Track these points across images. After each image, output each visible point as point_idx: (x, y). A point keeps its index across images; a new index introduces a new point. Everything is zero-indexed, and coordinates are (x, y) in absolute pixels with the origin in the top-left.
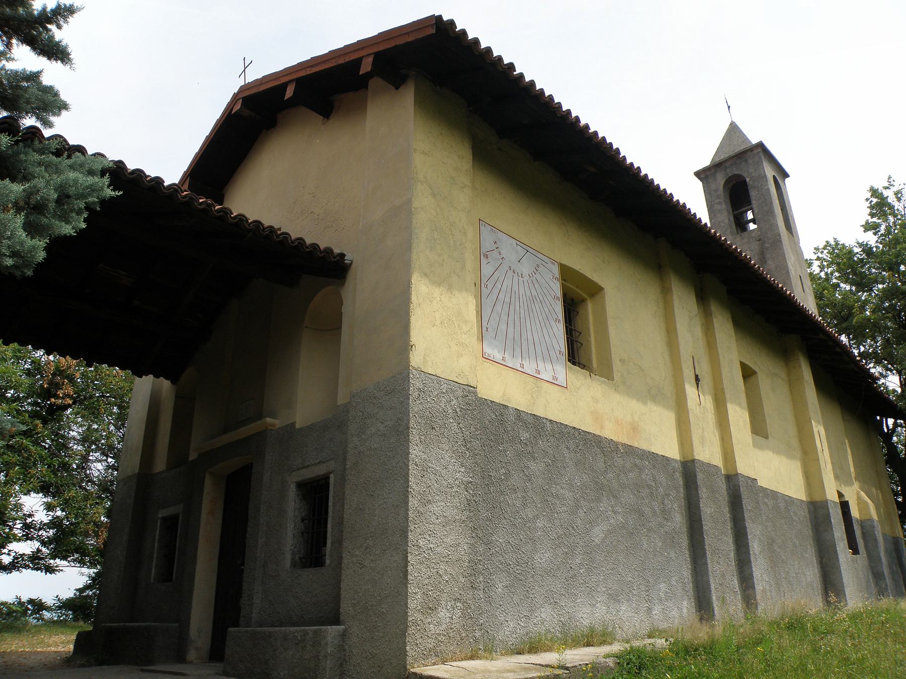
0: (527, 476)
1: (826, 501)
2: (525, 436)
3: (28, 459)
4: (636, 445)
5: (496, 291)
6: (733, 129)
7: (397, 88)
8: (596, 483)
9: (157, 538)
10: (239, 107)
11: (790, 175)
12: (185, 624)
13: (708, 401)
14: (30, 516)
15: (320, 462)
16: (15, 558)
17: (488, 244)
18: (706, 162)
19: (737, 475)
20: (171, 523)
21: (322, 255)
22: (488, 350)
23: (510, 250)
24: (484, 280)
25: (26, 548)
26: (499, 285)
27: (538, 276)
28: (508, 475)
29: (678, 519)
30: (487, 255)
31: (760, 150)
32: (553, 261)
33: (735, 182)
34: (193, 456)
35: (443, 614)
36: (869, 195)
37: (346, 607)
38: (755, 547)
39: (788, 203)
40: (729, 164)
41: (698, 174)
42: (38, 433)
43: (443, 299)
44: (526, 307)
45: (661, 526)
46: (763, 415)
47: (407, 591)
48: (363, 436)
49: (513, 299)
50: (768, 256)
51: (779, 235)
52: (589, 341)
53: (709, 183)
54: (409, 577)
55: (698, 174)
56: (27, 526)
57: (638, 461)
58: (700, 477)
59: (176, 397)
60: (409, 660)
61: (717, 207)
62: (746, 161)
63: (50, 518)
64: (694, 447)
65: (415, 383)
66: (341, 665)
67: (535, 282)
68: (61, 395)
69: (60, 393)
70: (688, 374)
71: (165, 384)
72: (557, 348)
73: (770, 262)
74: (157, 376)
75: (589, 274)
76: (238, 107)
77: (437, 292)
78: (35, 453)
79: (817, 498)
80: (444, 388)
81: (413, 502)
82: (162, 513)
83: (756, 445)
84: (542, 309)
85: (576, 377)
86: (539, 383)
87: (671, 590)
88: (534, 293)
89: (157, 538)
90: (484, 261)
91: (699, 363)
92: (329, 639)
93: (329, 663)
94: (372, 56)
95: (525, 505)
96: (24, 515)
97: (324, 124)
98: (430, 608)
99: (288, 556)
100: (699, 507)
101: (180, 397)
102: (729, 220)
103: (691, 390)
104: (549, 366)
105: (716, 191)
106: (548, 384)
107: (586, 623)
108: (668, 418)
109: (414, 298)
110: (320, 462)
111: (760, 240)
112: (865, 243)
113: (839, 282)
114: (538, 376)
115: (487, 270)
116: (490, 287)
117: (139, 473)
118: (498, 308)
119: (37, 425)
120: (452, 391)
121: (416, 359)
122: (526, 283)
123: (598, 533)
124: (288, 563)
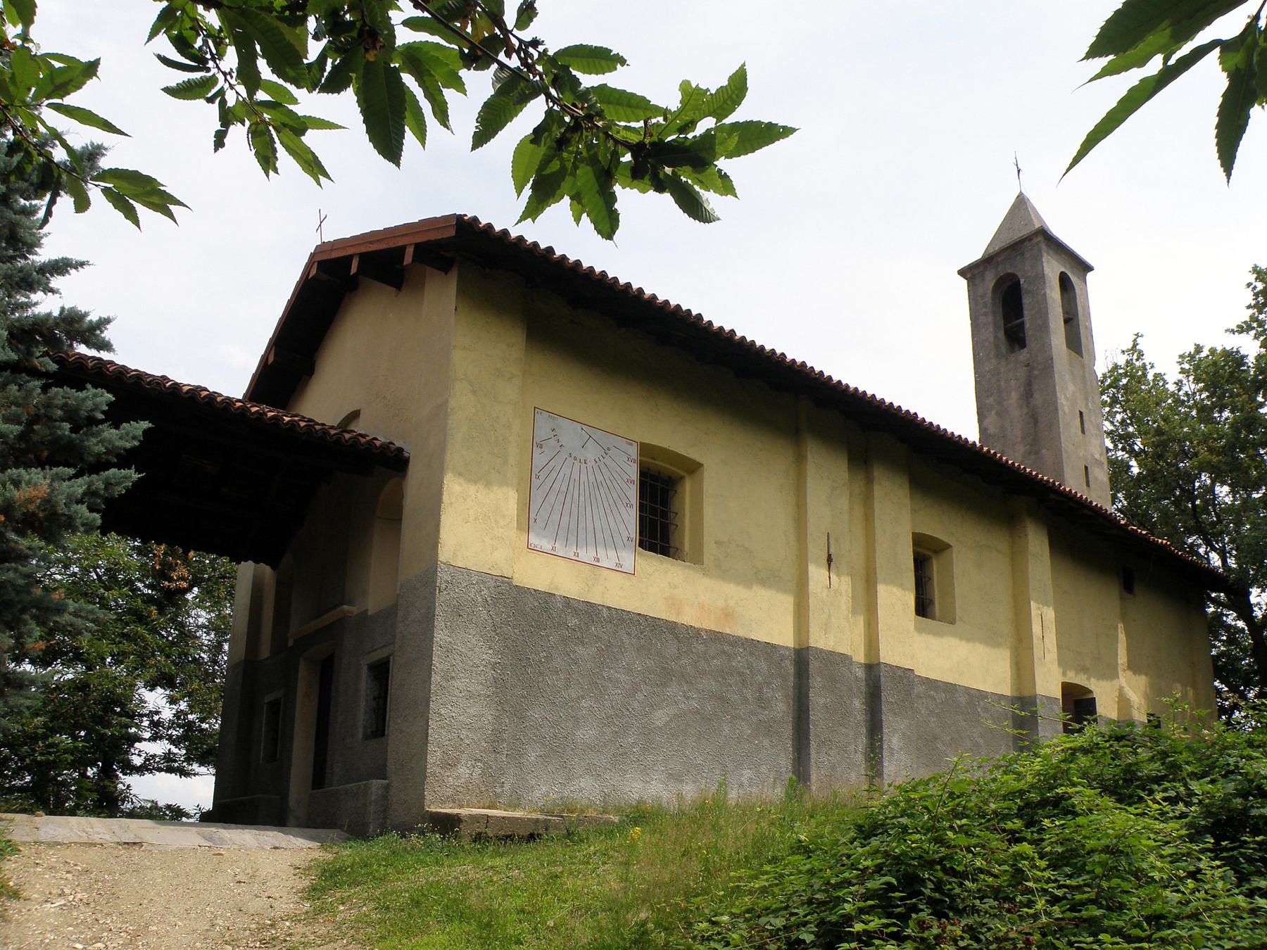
0: (573, 659)
1: (1035, 696)
2: (573, 622)
3: (145, 648)
4: (728, 631)
5: (549, 482)
6: (1021, 205)
7: (446, 274)
8: (664, 668)
9: (264, 722)
10: (315, 272)
11: (1095, 268)
12: (284, 796)
13: (843, 584)
14: (157, 713)
15: (385, 646)
16: (147, 760)
17: (543, 431)
18: (976, 254)
19: (879, 664)
20: (275, 706)
21: (379, 451)
22: (534, 540)
23: (570, 435)
24: (535, 471)
25: (159, 748)
26: (554, 475)
27: (608, 461)
28: (549, 658)
29: (781, 707)
30: (541, 445)
31: (1040, 238)
32: (630, 441)
33: (1010, 283)
34: (290, 644)
35: (462, 770)
36: (1252, 278)
37: (391, 767)
38: (894, 741)
41: (962, 273)
42: (153, 621)
43: (479, 495)
44: (587, 494)
45: (752, 713)
47: (427, 749)
48: (407, 623)
49: (571, 488)
50: (1035, 387)
51: (1052, 359)
52: (683, 523)
53: (976, 285)
54: (429, 738)
55: (962, 273)
56: (155, 724)
57: (727, 648)
58: (814, 665)
59: (277, 583)
60: (427, 802)
61: (982, 319)
62: (1022, 254)
63: (174, 712)
64: (811, 634)
65: (443, 576)
66: (384, 811)
67: (603, 467)
68: (175, 578)
69: (174, 575)
70: (816, 550)
71: (267, 570)
72: (625, 534)
73: (1036, 395)
74: (256, 562)
75: (682, 451)
76: (313, 272)
77: (472, 489)
78: (151, 642)
79: (1026, 693)
80: (475, 579)
81: (436, 678)
82: (268, 698)
83: (919, 629)
84: (608, 494)
85: (653, 564)
86: (597, 570)
87: (758, 777)
88: (600, 478)
89: (264, 722)
90: (537, 451)
91: (837, 540)
92: (373, 789)
93: (372, 808)
94: (413, 246)
95: (567, 687)
96: (150, 711)
97: (396, 296)
98: (450, 764)
99: (361, 730)
100: (808, 697)
101: (280, 583)
102: (996, 337)
103: (817, 574)
104: (612, 553)
105: (983, 296)
107: (636, 796)
108: (785, 603)
109: (445, 498)
110: (385, 646)
111: (1028, 365)
112: (1235, 350)
114: (597, 564)
115: (540, 460)
116: (542, 477)
117: (245, 660)
118: (552, 498)
119: (151, 612)
120: (483, 582)
121: (444, 554)
122: (590, 470)
123: (660, 717)
124: (360, 736)
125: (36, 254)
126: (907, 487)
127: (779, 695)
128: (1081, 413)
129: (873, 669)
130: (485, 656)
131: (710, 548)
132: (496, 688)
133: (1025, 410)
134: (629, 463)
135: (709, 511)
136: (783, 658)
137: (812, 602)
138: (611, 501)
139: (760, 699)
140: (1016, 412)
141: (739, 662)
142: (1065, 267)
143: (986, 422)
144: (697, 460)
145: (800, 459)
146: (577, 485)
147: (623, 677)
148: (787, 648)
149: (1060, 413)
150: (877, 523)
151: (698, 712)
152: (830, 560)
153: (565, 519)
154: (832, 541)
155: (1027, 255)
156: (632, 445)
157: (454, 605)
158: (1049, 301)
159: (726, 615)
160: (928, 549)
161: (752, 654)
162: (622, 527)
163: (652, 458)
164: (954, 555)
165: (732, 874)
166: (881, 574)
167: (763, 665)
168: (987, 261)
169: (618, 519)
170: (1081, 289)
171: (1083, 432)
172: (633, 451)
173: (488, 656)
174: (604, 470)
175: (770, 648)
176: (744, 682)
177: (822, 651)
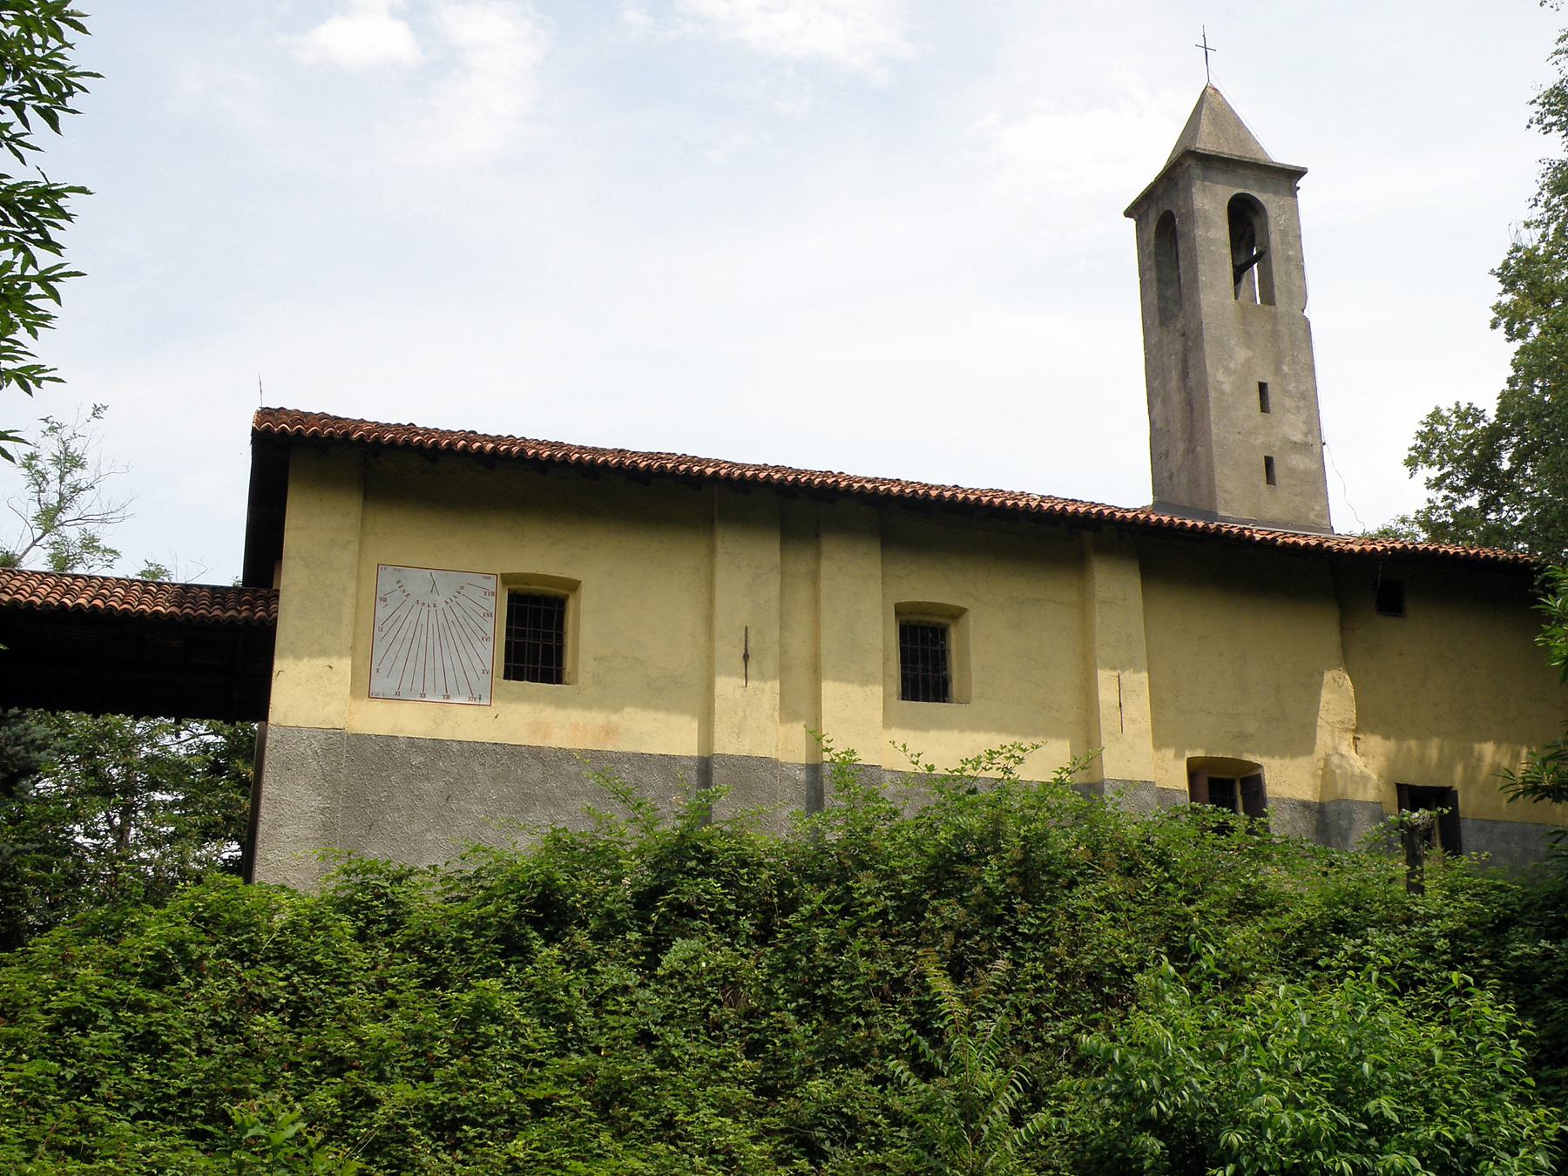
2: (417, 760)
6: (1209, 106)
31: (1190, 162)
32: (487, 576)
39: (1284, 233)
40: (1161, 191)
41: (1128, 214)
44: (436, 636)
46: (970, 670)
49: (418, 632)
50: (1190, 363)
55: (1128, 214)
58: (718, 773)
62: (1176, 184)
70: (728, 650)
72: (479, 668)
73: (1191, 375)
88: (451, 617)
95: (410, 822)
106: (467, 707)
111: (1183, 335)
113: (1529, 340)
115: (383, 613)
116: (385, 630)
118: (396, 646)
122: (440, 613)
125: (35, 334)
126: (876, 556)
128: (1263, 387)
130: (313, 803)
132: (325, 830)
133: (1183, 394)
134: (487, 597)
138: (464, 638)
140: (1177, 399)
143: (1155, 412)
144: (573, 577)
146: (424, 631)
147: (474, 808)
148: (691, 758)
149: (1212, 395)
152: (746, 657)
153: (411, 664)
156: (489, 578)
157: (284, 761)
158: (1201, 245)
159: (608, 732)
160: (940, 616)
162: (476, 661)
163: (526, 584)
164: (972, 622)
166: (826, 662)
167: (657, 779)
171: (1264, 407)
172: (491, 585)
173: (316, 802)
174: (457, 610)
175: (666, 763)
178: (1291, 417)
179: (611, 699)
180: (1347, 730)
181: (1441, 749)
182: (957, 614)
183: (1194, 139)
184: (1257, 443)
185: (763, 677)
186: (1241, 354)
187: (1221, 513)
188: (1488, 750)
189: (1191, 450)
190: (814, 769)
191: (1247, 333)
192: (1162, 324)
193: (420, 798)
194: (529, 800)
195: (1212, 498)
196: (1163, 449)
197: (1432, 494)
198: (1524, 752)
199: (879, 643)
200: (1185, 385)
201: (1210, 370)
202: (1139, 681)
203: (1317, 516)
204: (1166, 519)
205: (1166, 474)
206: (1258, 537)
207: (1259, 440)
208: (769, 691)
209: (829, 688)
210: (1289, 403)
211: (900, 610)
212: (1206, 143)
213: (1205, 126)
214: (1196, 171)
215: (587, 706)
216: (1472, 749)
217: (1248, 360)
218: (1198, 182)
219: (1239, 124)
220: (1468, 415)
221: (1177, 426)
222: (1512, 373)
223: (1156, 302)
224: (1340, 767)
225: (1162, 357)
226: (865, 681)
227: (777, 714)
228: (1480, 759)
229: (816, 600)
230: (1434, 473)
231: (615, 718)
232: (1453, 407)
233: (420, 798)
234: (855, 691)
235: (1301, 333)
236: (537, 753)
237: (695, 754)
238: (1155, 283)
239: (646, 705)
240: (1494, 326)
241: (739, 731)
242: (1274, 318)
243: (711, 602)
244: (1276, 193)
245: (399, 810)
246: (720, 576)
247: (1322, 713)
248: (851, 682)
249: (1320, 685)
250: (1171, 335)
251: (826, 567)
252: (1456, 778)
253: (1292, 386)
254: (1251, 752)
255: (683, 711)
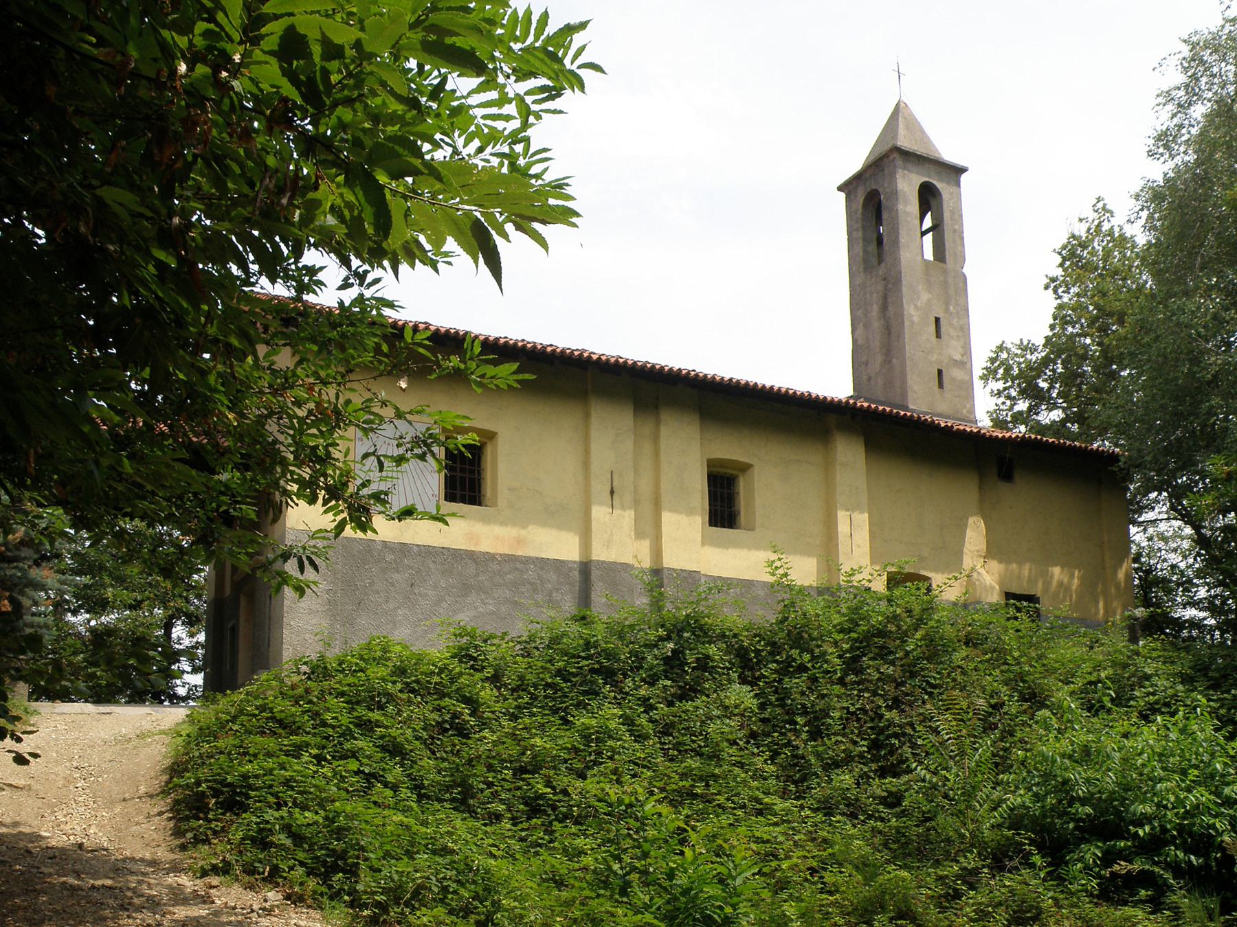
2: (389, 557)
4: (520, 553)
8: (464, 584)
31: (896, 155)
41: (840, 189)
50: (890, 300)
55: (840, 189)
58: (595, 574)
61: (855, 234)
62: (883, 170)
70: (600, 488)
73: (890, 308)
95: (387, 602)
102: (865, 251)
105: (856, 212)
111: (885, 279)
127: (568, 598)
128: (937, 320)
129: (657, 572)
131: (503, 494)
133: (883, 321)
135: (502, 467)
136: (570, 570)
137: (594, 525)
138: (418, 470)
139: (550, 601)
140: (877, 325)
141: (531, 574)
142: (924, 176)
143: (857, 333)
145: (587, 416)
147: (430, 593)
148: (575, 562)
149: (907, 323)
150: (663, 457)
151: (493, 613)
152: (612, 492)
154: (615, 477)
155: (886, 171)
158: (902, 217)
160: (734, 469)
161: (542, 569)
162: (428, 489)
164: (756, 473)
165: (19, 574)
166: (665, 499)
167: (553, 576)
168: (858, 178)
169: (425, 482)
170: (951, 194)
171: (938, 335)
175: (558, 565)
176: (535, 590)
177: (603, 562)
178: (954, 343)
179: (520, 519)
180: (980, 556)
181: (1030, 570)
182: (745, 468)
183: (895, 136)
184: (933, 359)
185: (623, 508)
186: (925, 296)
187: (911, 407)
188: (1056, 571)
189: (887, 361)
190: (657, 572)
191: (929, 281)
192: (865, 270)
193: (392, 585)
194: (466, 589)
195: (904, 394)
196: (864, 359)
197: (995, 400)
198: (1077, 573)
199: (699, 487)
200: (885, 315)
201: (905, 306)
202: (863, 518)
203: (968, 412)
204: (888, 409)
205: (865, 377)
206: (943, 425)
207: (934, 358)
208: (627, 518)
209: (666, 517)
210: (953, 333)
211: (711, 464)
212: (904, 142)
213: (902, 131)
214: (899, 162)
215: (504, 524)
216: (1047, 571)
217: (929, 300)
218: (900, 171)
219: (923, 132)
220: (1028, 348)
221: (876, 344)
222: (1052, 322)
223: (861, 253)
224: (978, 580)
225: (865, 294)
226: (690, 512)
227: (633, 533)
228: (1052, 577)
229: (657, 453)
230: (1000, 385)
231: (523, 532)
232: (1018, 343)
233: (392, 585)
234: (683, 519)
235: (961, 284)
236: (471, 555)
237: (577, 559)
238: (861, 241)
239: (544, 524)
240: (1047, 287)
241: (608, 544)
242: (945, 272)
243: (587, 452)
244: (948, 183)
245: (378, 593)
246: (594, 434)
247: (967, 545)
248: (680, 513)
249: (966, 526)
250: (873, 280)
251: (664, 431)
252: (1037, 590)
253: (955, 321)
254: (925, 569)
255: (569, 529)
